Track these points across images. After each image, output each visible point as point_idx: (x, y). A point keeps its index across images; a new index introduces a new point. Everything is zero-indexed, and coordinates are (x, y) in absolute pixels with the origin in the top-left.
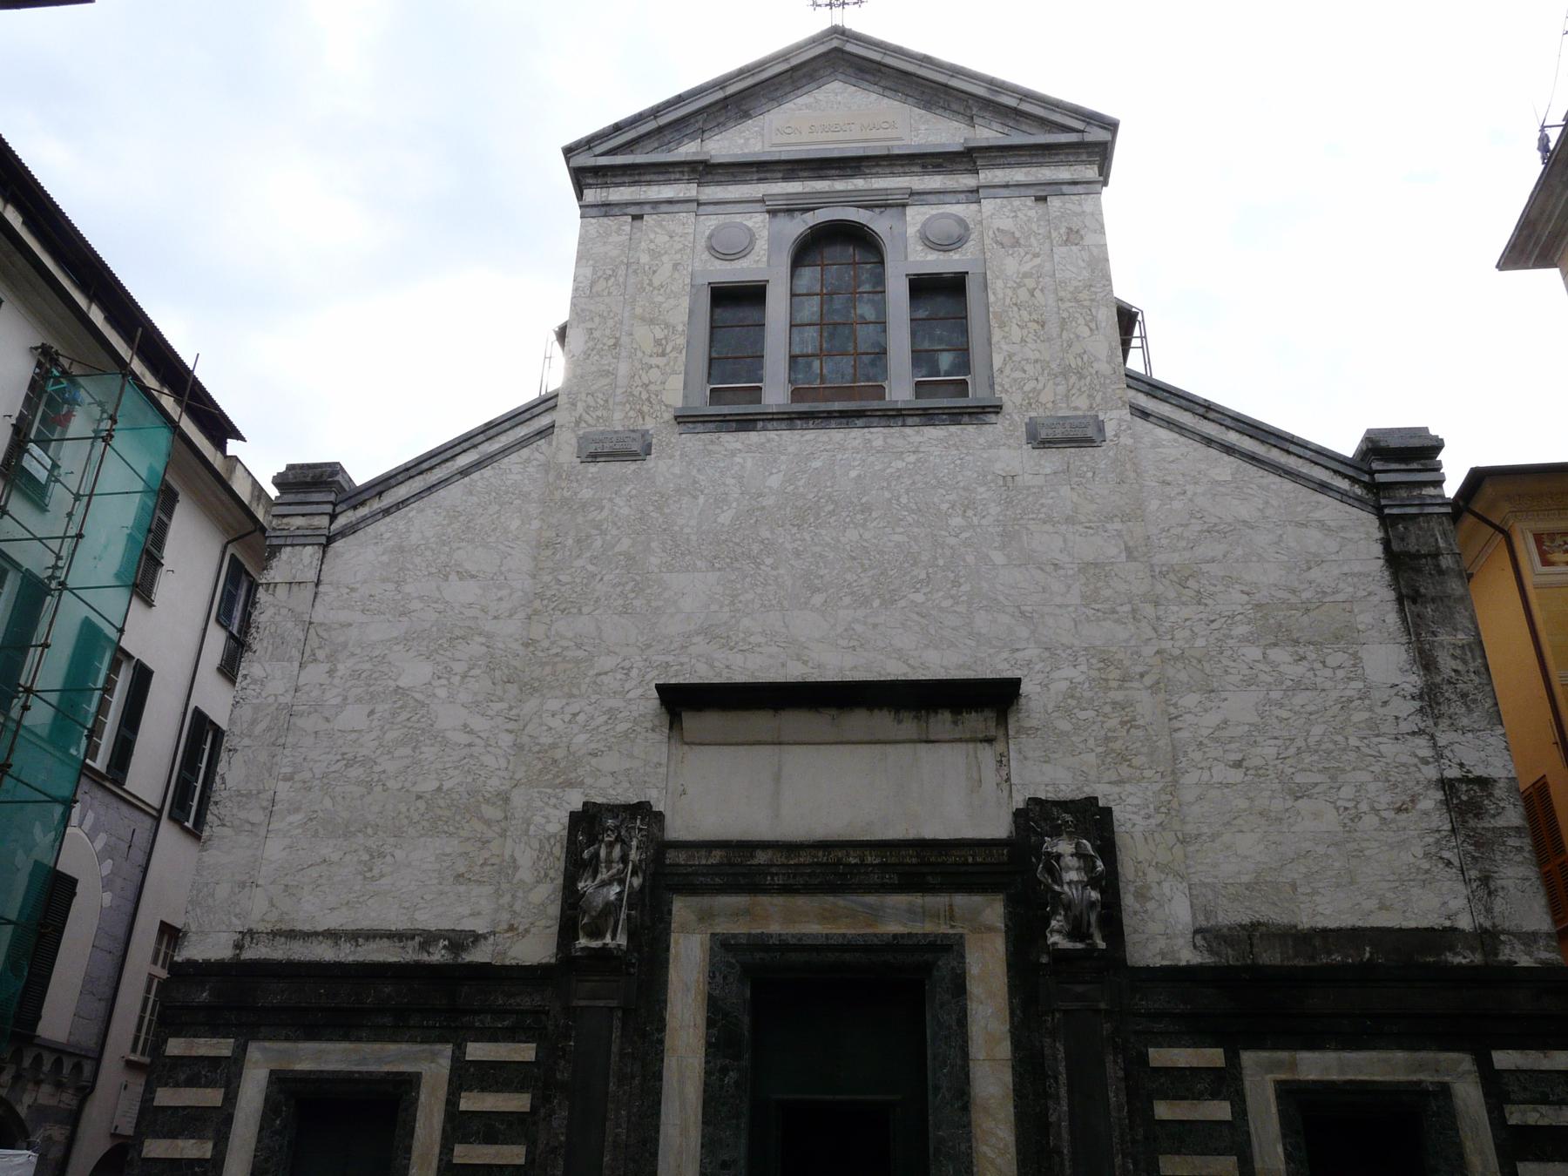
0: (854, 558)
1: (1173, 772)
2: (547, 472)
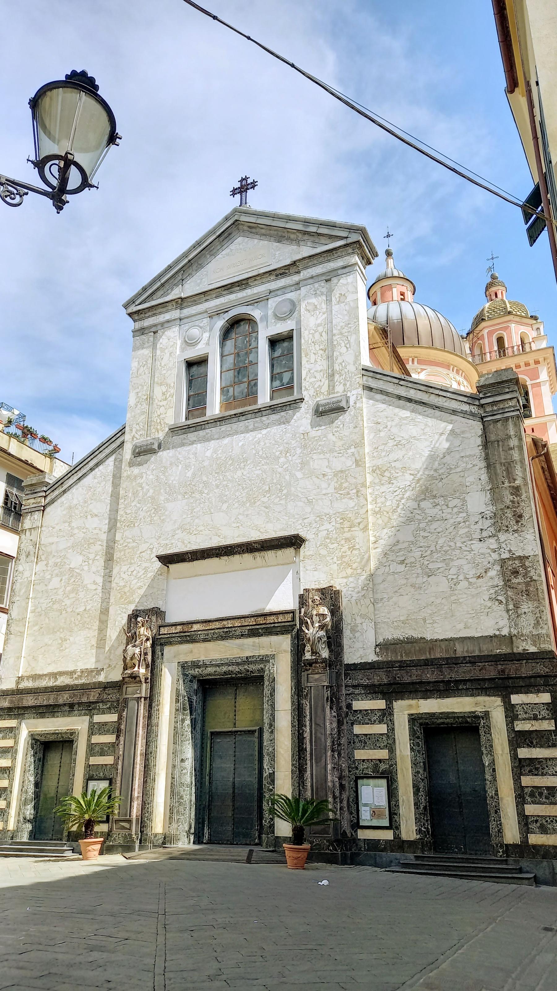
0: (240, 485)
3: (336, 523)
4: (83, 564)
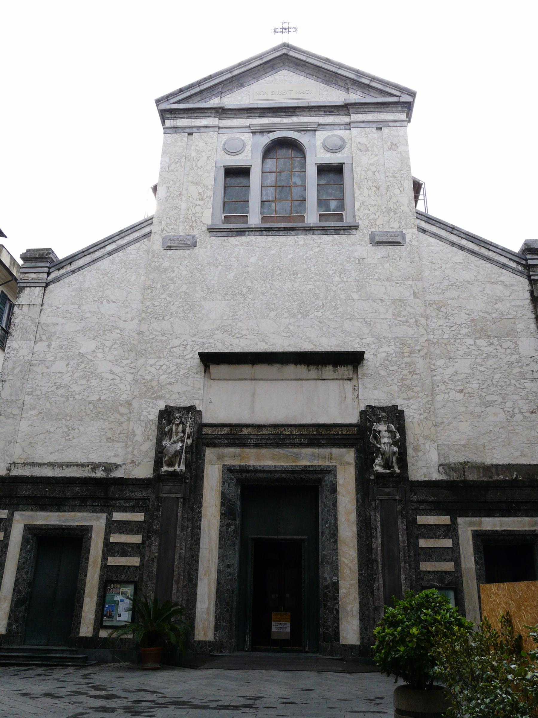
0: (289, 296)
1: (432, 395)
2: (148, 254)
3: (395, 347)
4: (97, 351)
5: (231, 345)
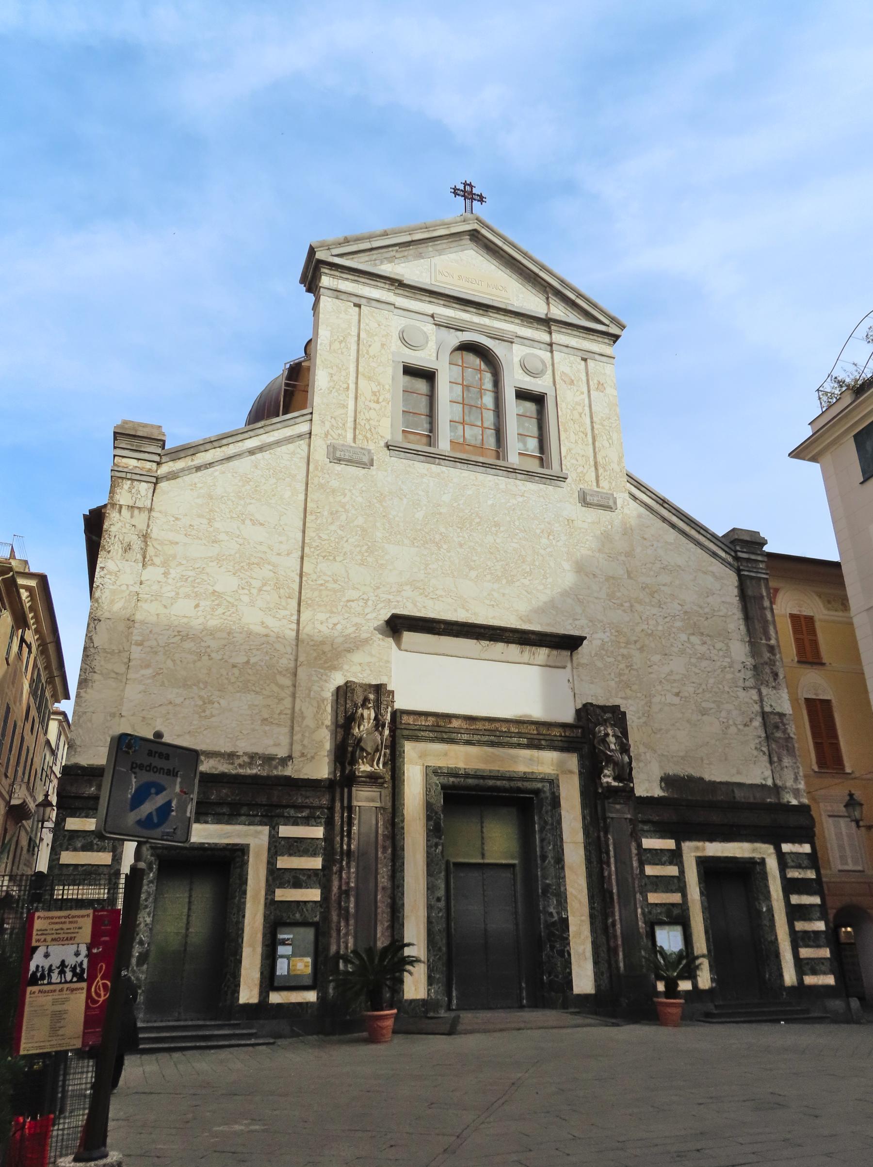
0: (491, 553)
5: (424, 607)
